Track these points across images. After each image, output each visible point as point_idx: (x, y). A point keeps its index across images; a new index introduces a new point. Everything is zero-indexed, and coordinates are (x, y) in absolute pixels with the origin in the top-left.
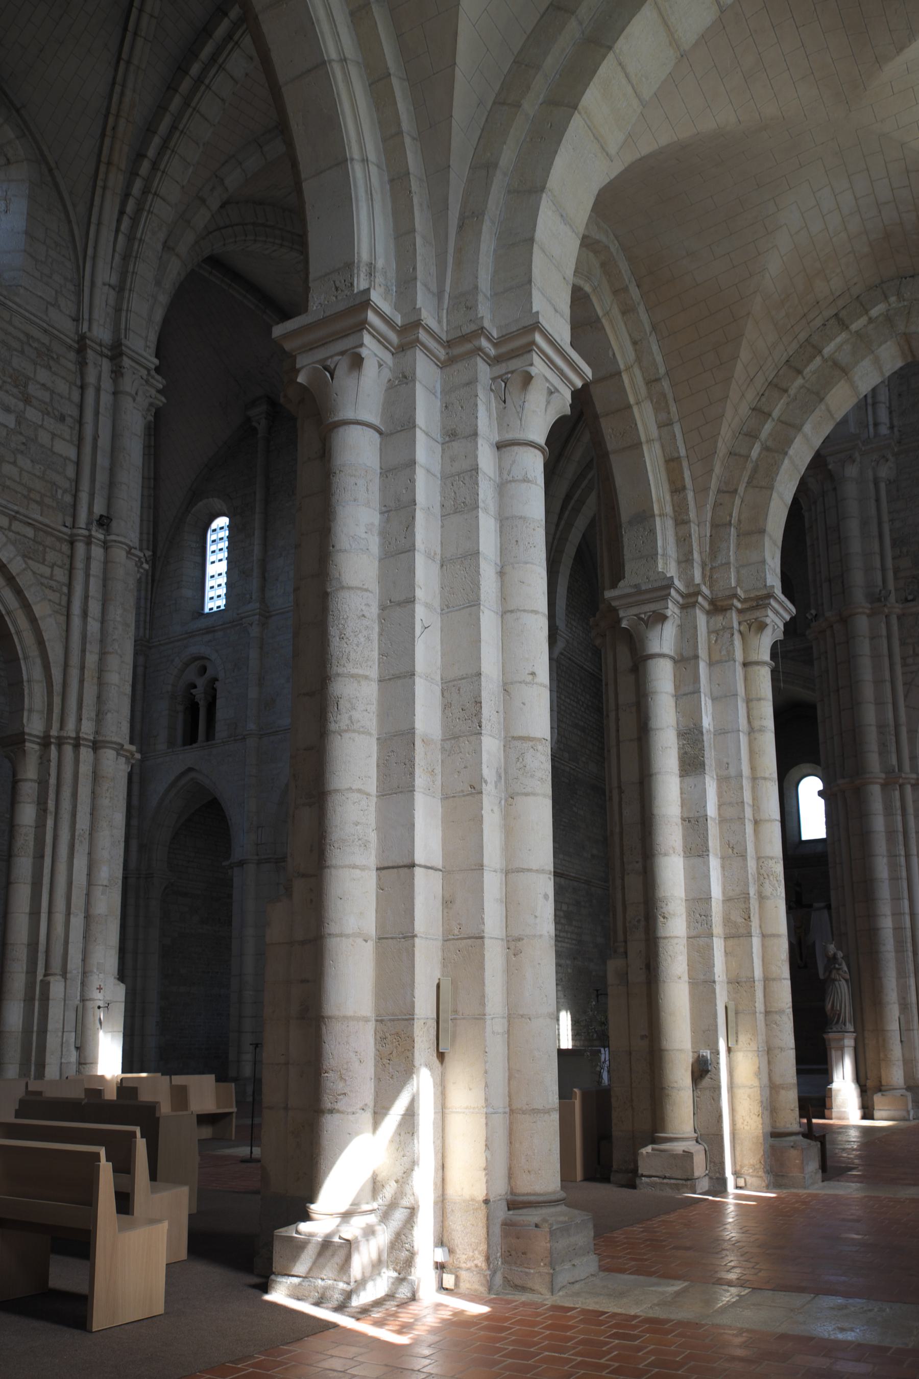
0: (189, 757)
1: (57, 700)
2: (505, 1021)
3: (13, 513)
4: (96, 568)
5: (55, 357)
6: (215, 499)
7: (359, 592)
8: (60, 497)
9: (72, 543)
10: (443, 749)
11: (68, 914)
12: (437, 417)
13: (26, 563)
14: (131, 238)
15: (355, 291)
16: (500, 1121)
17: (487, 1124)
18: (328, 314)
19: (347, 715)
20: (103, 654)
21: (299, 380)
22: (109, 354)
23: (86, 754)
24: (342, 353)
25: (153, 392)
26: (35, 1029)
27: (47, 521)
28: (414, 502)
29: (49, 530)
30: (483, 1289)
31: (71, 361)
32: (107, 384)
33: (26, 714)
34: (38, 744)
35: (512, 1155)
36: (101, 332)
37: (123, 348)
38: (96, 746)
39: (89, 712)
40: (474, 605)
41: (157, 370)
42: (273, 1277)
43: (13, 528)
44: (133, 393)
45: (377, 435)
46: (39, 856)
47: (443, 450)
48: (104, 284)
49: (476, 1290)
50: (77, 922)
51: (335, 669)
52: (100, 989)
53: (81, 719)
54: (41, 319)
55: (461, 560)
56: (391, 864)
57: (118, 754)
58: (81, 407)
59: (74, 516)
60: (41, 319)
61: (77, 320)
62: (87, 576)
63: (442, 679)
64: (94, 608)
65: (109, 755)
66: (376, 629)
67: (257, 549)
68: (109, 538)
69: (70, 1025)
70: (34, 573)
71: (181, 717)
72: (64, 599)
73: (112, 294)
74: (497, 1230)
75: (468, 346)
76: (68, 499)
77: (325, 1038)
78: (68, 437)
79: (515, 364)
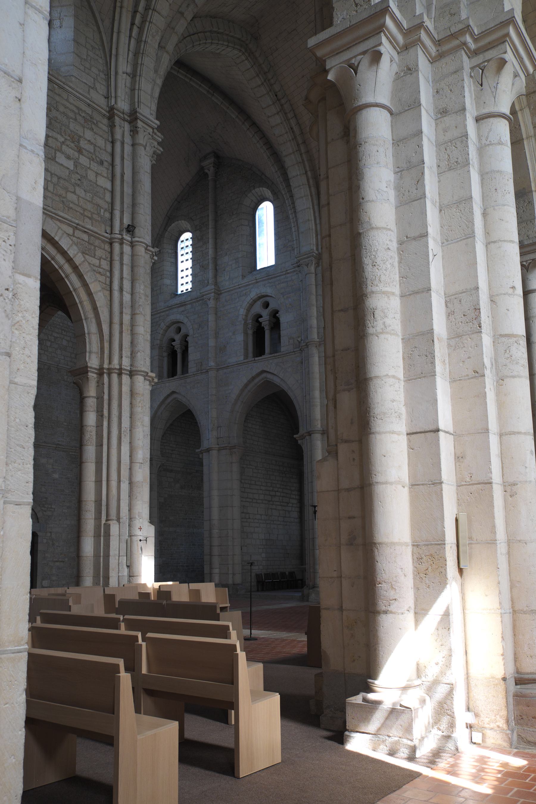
0: (173, 384)
1: (106, 345)
2: (506, 545)
3: (75, 225)
4: (127, 259)
5: (95, 122)
6: (183, 221)
7: (384, 231)
8: (102, 214)
9: (111, 244)
10: (449, 346)
11: (119, 481)
12: (431, 101)
13: (84, 257)
14: (139, 41)
15: (372, 4)
16: (508, 618)
17: (502, 621)
18: (353, 22)
19: (381, 322)
20: (133, 315)
21: (329, 77)
22: (129, 119)
23: (126, 379)
24: (364, 53)
25: (156, 144)
26: (102, 554)
27: (95, 230)
28: (423, 162)
29: (97, 235)
30: (505, 744)
31: (105, 125)
32: (128, 140)
33: (87, 354)
34: (96, 373)
35: (516, 644)
36: (123, 105)
37: (138, 114)
38: (131, 374)
39: (126, 352)
40: (470, 237)
41: (159, 129)
42: (347, 733)
43: (75, 234)
44: (144, 144)
45: (389, 115)
46: (100, 445)
47: (437, 124)
48: (124, 73)
49: (500, 745)
50: (125, 486)
51: (369, 289)
52: (140, 529)
53: (122, 357)
54: (86, 97)
55: (457, 205)
56: (418, 431)
57: (145, 379)
58: (113, 155)
59: (112, 226)
60: (86, 97)
61: (107, 97)
62: (122, 264)
63: (445, 294)
64: (127, 285)
65: (139, 379)
66: (397, 259)
67: (211, 252)
68: (134, 239)
69: (123, 552)
70: (89, 264)
71: (166, 359)
72: (108, 280)
73: (129, 79)
74: (511, 699)
75: (456, 43)
76: (107, 215)
77: (377, 558)
78: (106, 175)
79: (489, 55)
